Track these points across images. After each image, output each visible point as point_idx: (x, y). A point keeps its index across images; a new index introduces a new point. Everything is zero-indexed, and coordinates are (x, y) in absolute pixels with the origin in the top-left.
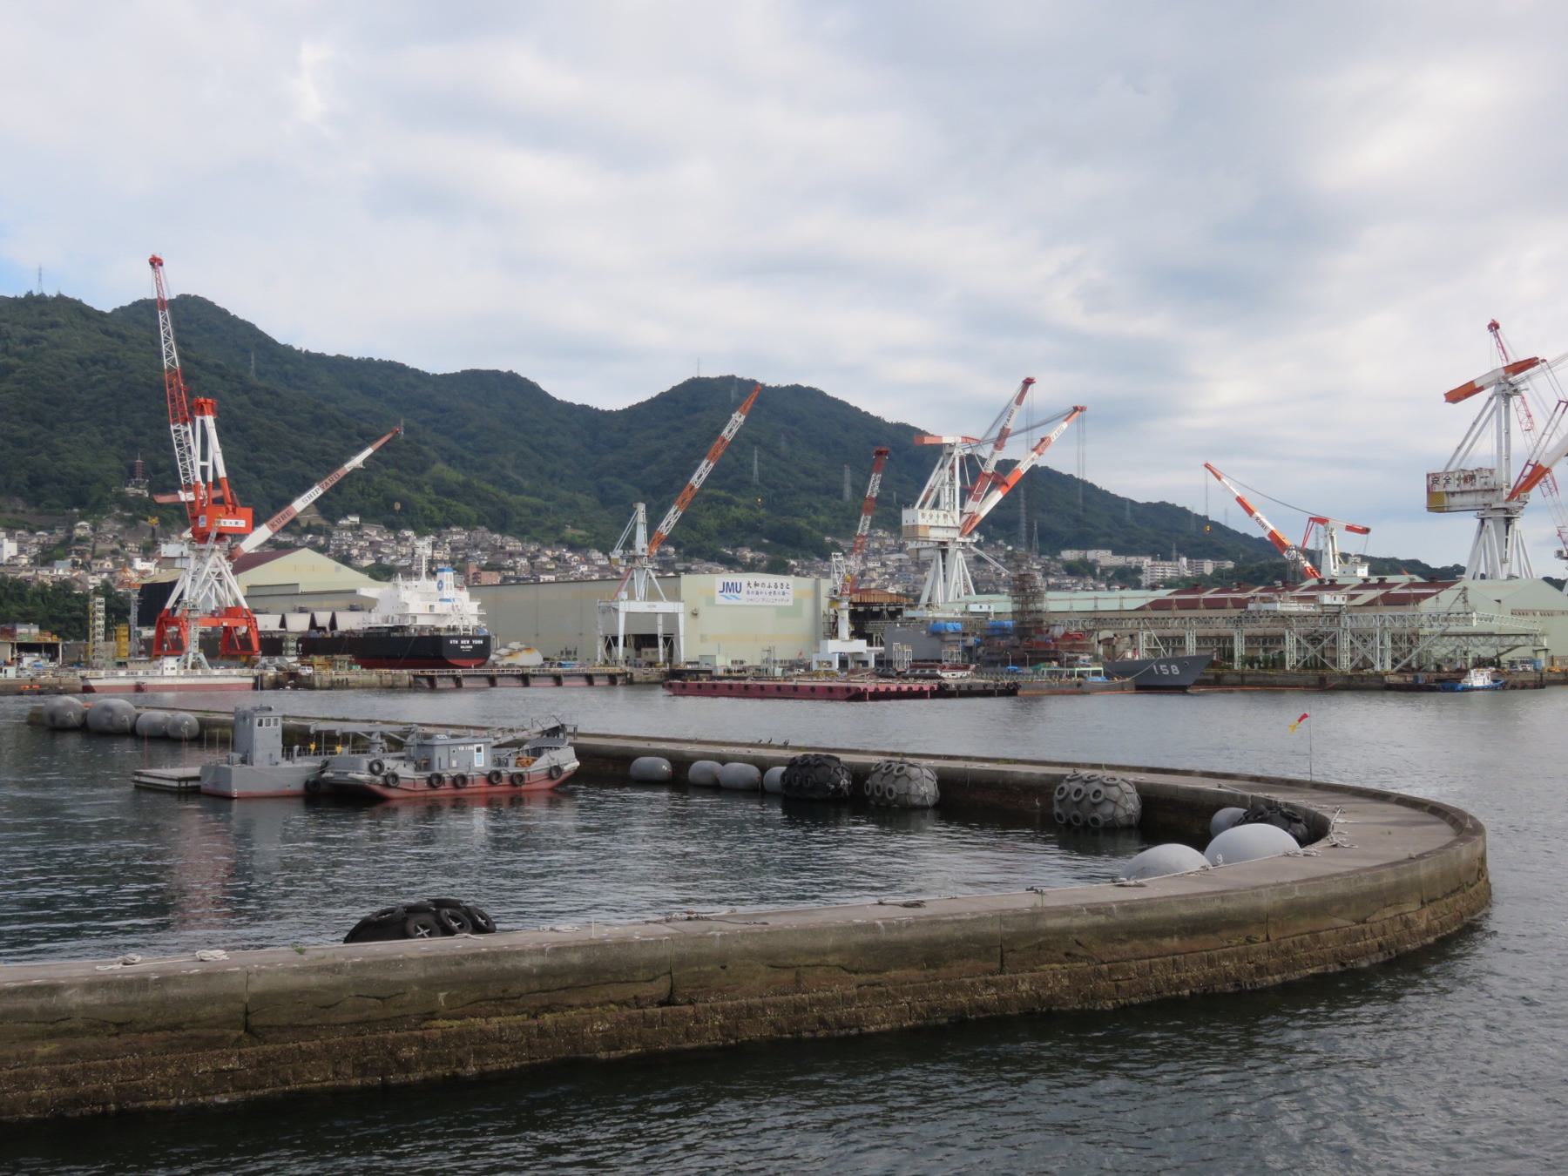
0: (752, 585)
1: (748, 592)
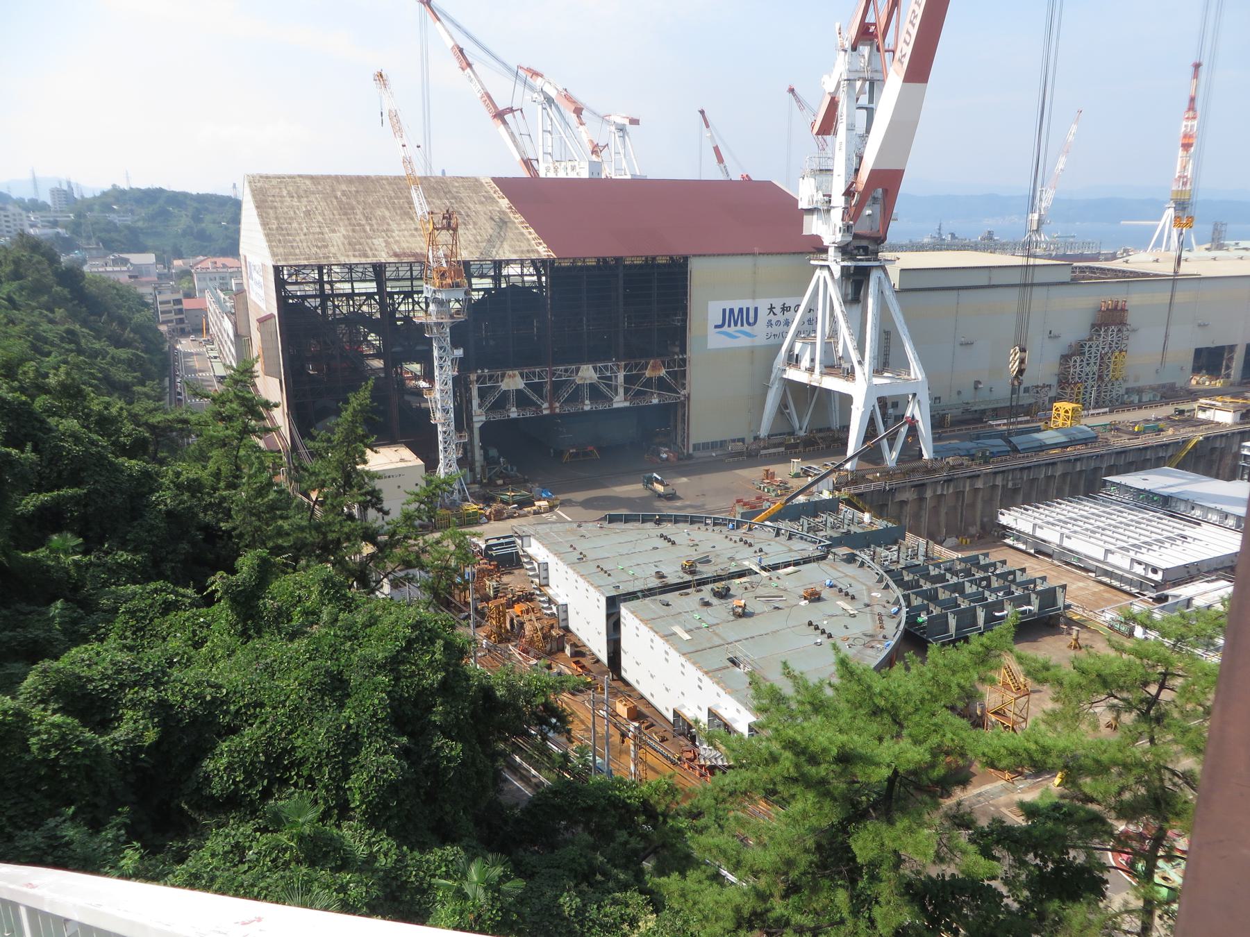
0: (778, 310)
1: (770, 323)
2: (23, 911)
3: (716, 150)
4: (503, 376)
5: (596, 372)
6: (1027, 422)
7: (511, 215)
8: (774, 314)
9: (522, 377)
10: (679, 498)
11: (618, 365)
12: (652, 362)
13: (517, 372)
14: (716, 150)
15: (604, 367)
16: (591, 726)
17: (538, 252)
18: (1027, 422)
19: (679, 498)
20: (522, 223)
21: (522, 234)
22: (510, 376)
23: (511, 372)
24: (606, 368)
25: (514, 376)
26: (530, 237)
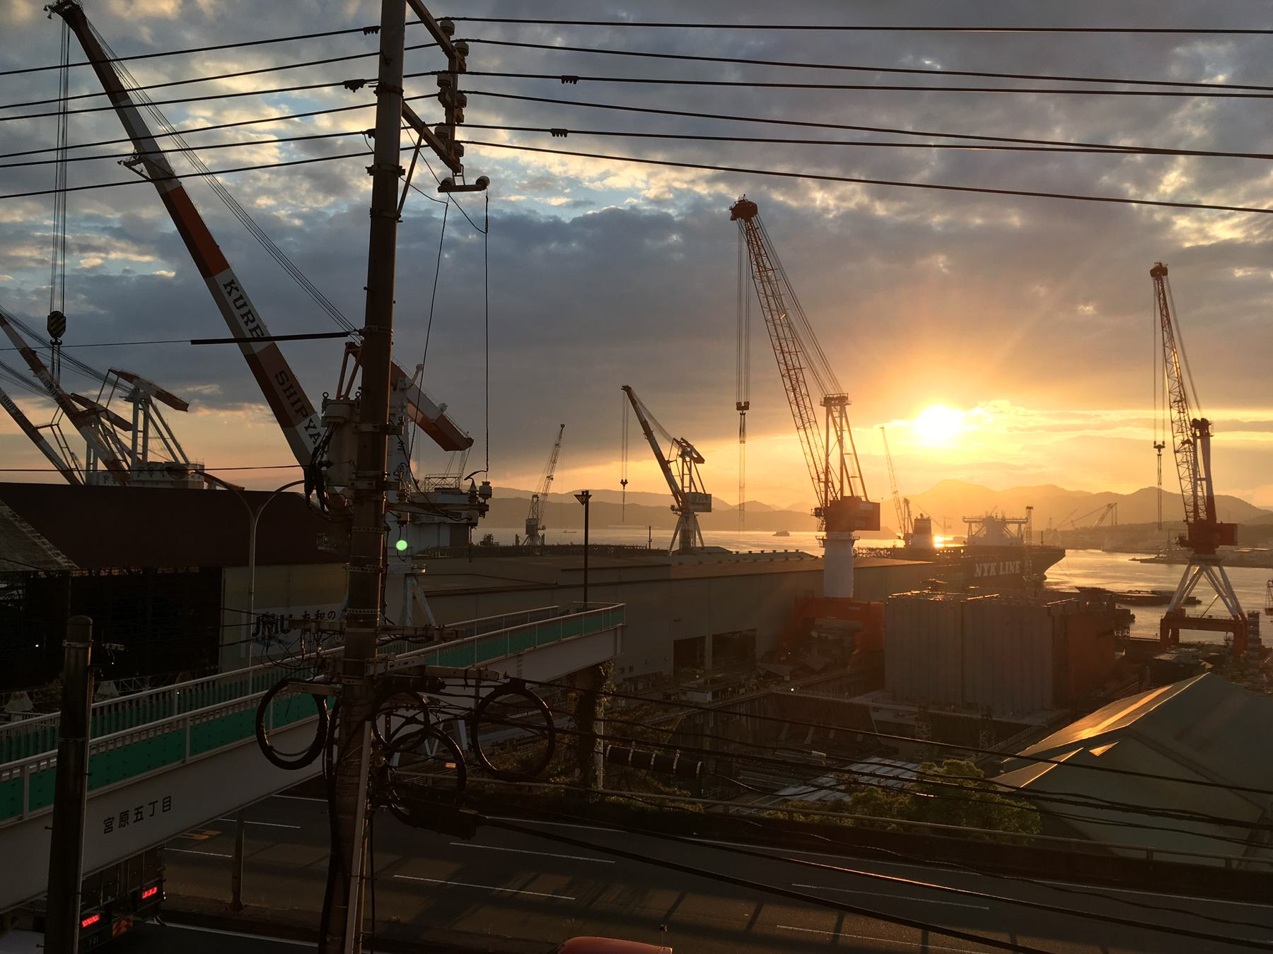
2: (83, 913)
3: (194, 342)
4: (8, 697)
5: (118, 688)
6: (365, 824)
7: (17, 524)
8: (306, 612)
9: (31, 698)
10: (1199, 602)
11: (142, 680)
12: (181, 674)
13: (25, 692)
14: (194, 342)
15: (127, 682)
16: (636, 722)
17: (58, 563)
18: (365, 824)
19: (1199, 602)
20: (32, 532)
21: (35, 544)
22: (16, 697)
23: (17, 693)
24: (129, 683)
25: (22, 696)
26: (44, 547)
